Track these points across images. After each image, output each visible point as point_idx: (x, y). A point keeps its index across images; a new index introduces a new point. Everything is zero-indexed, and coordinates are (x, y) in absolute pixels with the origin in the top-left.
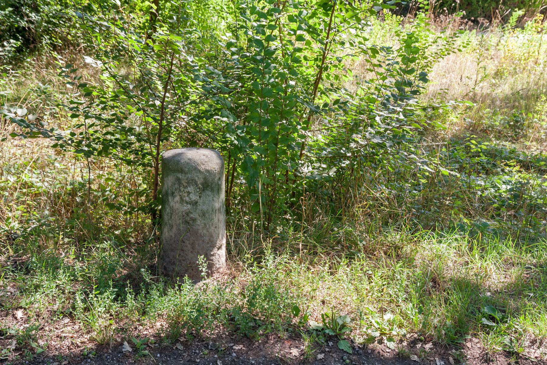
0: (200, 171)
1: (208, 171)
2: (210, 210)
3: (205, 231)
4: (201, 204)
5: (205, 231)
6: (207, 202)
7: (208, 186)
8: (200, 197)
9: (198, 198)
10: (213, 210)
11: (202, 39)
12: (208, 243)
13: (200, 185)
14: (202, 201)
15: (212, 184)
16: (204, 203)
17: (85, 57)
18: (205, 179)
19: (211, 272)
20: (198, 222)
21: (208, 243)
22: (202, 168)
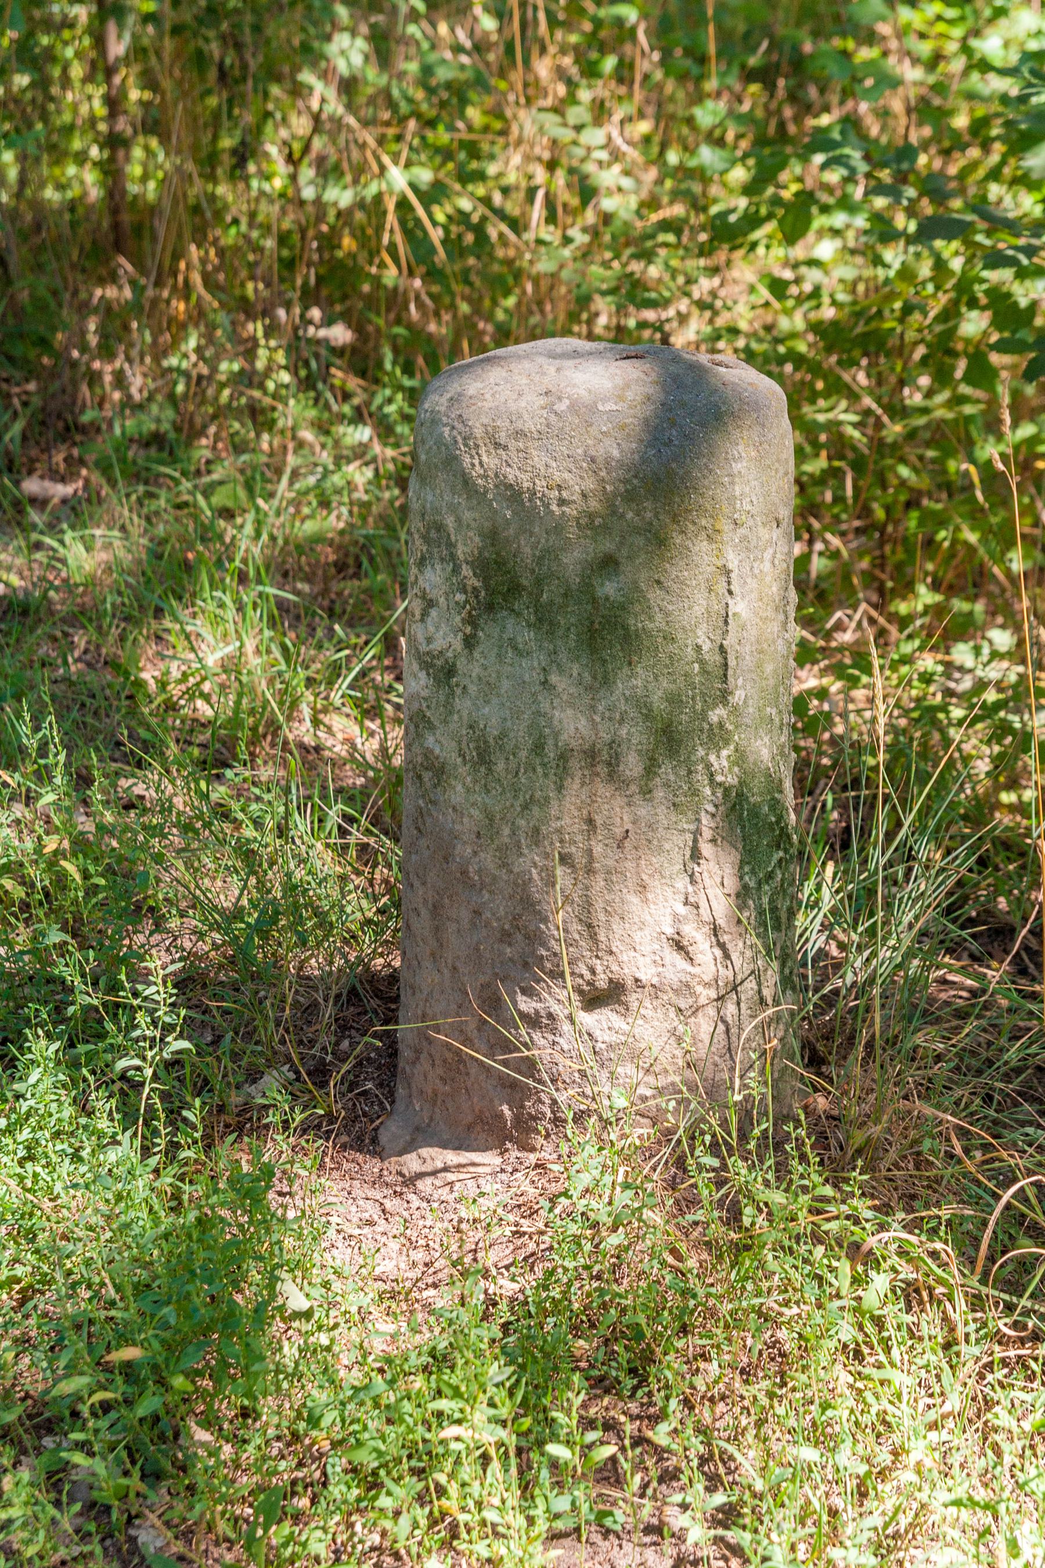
0: (466, 481)
1: (513, 494)
2: (520, 734)
3: (488, 859)
4: (473, 689)
5: (488, 859)
6: (506, 685)
7: (515, 589)
8: (470, 642)
9: (458, 644)
10: (538, 748)
11: (111, 938)
12: (506, 937)
13: (466, 571)
14: (476, 671)
15: (539, 582)
16: (489, 689)
17: (814, 575)
18: (492, 536)
19: (518, 1119)
20: (456, 793)
21: (506, 937)
22: (484, 464)
